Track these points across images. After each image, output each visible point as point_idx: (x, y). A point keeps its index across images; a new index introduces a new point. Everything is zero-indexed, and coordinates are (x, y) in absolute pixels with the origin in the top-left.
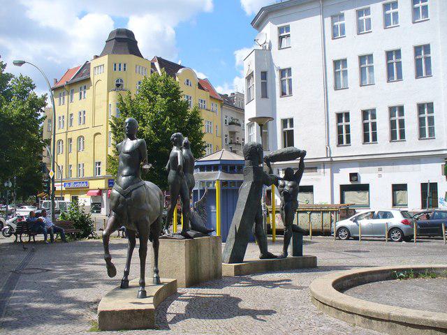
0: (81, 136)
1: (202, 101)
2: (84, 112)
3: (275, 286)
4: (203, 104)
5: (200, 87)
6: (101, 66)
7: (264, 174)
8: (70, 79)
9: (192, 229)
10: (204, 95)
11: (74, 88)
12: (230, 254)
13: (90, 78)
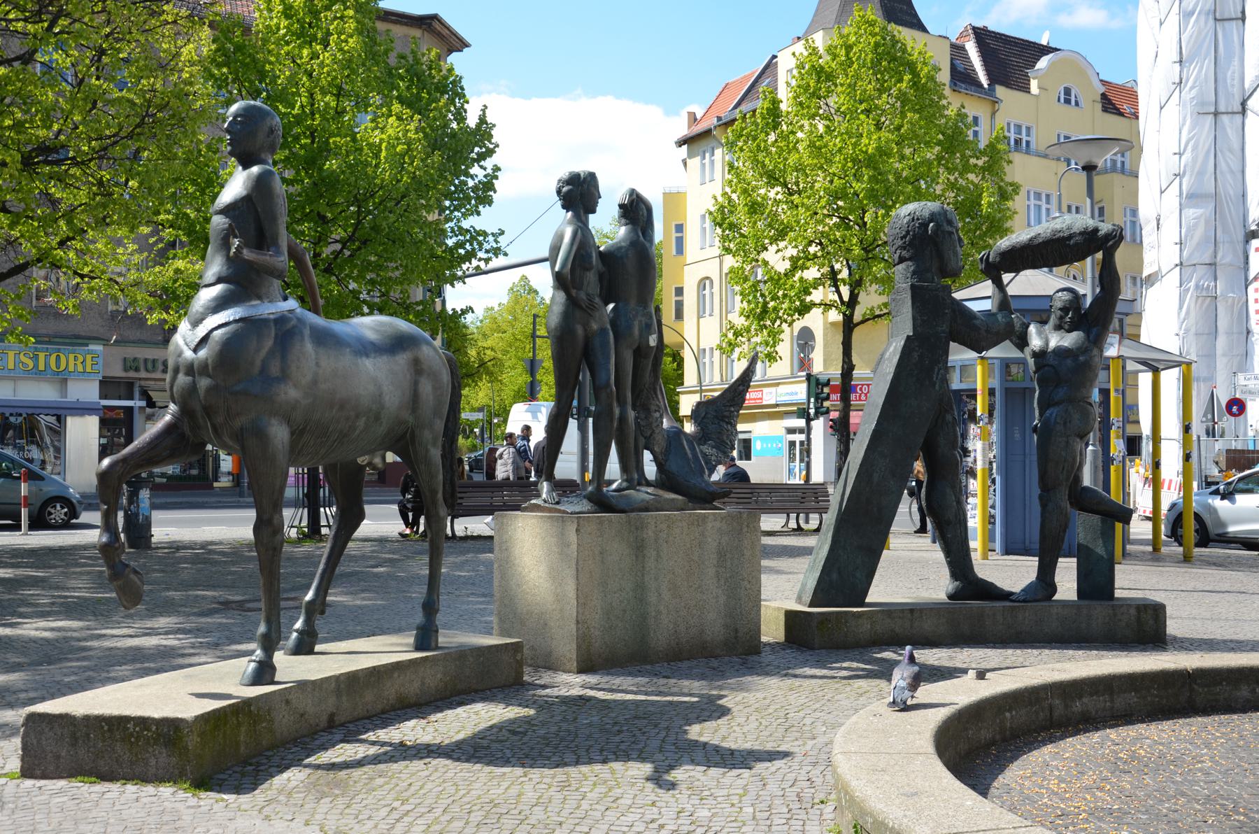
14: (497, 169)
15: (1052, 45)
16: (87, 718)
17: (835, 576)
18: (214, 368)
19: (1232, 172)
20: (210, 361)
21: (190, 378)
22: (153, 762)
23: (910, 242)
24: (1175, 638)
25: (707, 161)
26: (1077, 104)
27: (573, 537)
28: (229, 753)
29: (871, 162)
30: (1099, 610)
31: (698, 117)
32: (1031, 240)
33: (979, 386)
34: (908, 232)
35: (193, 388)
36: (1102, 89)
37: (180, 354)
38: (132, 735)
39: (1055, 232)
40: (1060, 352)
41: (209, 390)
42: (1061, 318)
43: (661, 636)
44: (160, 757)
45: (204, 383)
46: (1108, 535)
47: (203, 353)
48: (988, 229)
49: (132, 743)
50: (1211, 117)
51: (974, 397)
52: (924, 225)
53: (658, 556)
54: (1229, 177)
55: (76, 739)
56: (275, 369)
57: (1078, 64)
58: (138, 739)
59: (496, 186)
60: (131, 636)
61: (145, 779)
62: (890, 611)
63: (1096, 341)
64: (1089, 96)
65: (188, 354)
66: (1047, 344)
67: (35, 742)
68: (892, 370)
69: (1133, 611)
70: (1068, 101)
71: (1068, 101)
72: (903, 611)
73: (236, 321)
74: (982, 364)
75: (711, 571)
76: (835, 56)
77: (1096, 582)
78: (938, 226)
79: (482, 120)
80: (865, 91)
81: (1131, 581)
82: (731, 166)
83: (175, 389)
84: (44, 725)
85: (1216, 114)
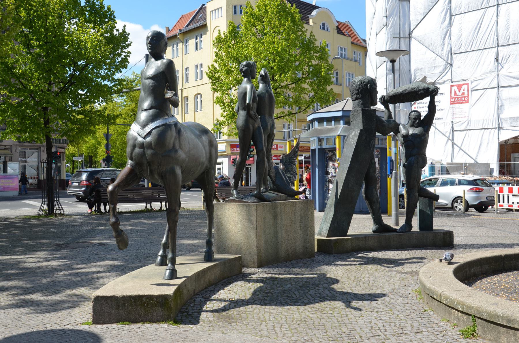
0: (199, 94)
1: (341, 48)
2: (201, 65)
3: (403, 264)
4: (343, 53)
5: (339, 31)
6: (218, 9)
7: (379, 119)
8: (183, 26)
9: (273, 190)
10: (344, 41)
11: (189, 35)
12: (329, 224)
13: (206, 25)
14: (129, 52)
15: (317, 5)
16: (124, 297)
17: (336, 225)
18: (155, 145)
19: (406, 61)
20: (153, 142)
21: (142, 150)
22: (155, 313)
23: (361, 91)
24: (458, 245)
25: (175, 48)
26: (327, 30)
27: (254, 213)
28: (182, 307)
29: (278, 54)
30: (429, 234)
31: (170, 29)
32: (403, 91)
33: (337, 147)
34: (360, 88)
35: (143, 155)
36: (337, 24)
37: (136, 139)
38: (145, 303)
39: (412, 89)
40: (413, 135)
41: (152, 155)
42: (414, 122)
43: (282, 253)
44: (159, 311)
45: (149, 152)
46: (431, 205)
47: (148, 139)
48: (324, 83)
49: (145, 306)
50: (398, 39)
51: (336, 151)
52: (366, 85)
53: (281, 219)
54: (404, 63)
55: (119, 306)
56: (177, 147)
57: (327, 13)
58: (148, 304)
59: (129, 61)
60: (38, 262)
61: (152, 321)
62: (358, 238)
63: (427, 130)
64: (332, 27)
65: (140, 139)
66: (408, 132)
67: (99, 309)
68: (355, 142)
69: (442, 235)
70: (324, 29)
71: (324, 29)
72: (362, 238)
73: (162, 125)
74: (339, 138)
75: (298, 224)
76: (260, 10)
77: (426, 223)
78: (371, 86)
79: (124, 31)
80: (275, 24)
81: (439, 223)
82: (217, 55)
83: (133, 155)
84: (103, 301)
85: (400, 38)
